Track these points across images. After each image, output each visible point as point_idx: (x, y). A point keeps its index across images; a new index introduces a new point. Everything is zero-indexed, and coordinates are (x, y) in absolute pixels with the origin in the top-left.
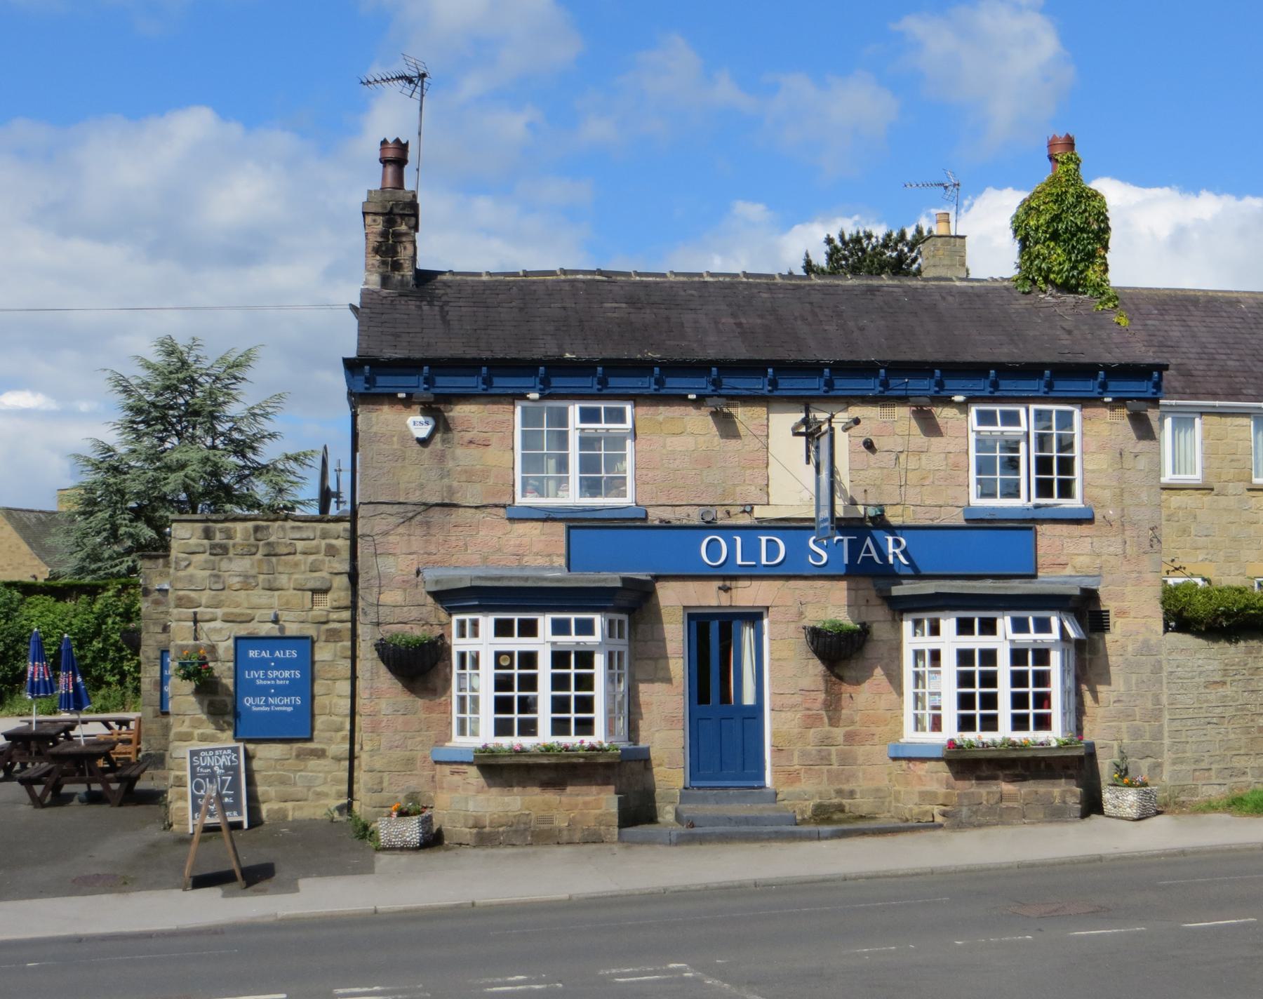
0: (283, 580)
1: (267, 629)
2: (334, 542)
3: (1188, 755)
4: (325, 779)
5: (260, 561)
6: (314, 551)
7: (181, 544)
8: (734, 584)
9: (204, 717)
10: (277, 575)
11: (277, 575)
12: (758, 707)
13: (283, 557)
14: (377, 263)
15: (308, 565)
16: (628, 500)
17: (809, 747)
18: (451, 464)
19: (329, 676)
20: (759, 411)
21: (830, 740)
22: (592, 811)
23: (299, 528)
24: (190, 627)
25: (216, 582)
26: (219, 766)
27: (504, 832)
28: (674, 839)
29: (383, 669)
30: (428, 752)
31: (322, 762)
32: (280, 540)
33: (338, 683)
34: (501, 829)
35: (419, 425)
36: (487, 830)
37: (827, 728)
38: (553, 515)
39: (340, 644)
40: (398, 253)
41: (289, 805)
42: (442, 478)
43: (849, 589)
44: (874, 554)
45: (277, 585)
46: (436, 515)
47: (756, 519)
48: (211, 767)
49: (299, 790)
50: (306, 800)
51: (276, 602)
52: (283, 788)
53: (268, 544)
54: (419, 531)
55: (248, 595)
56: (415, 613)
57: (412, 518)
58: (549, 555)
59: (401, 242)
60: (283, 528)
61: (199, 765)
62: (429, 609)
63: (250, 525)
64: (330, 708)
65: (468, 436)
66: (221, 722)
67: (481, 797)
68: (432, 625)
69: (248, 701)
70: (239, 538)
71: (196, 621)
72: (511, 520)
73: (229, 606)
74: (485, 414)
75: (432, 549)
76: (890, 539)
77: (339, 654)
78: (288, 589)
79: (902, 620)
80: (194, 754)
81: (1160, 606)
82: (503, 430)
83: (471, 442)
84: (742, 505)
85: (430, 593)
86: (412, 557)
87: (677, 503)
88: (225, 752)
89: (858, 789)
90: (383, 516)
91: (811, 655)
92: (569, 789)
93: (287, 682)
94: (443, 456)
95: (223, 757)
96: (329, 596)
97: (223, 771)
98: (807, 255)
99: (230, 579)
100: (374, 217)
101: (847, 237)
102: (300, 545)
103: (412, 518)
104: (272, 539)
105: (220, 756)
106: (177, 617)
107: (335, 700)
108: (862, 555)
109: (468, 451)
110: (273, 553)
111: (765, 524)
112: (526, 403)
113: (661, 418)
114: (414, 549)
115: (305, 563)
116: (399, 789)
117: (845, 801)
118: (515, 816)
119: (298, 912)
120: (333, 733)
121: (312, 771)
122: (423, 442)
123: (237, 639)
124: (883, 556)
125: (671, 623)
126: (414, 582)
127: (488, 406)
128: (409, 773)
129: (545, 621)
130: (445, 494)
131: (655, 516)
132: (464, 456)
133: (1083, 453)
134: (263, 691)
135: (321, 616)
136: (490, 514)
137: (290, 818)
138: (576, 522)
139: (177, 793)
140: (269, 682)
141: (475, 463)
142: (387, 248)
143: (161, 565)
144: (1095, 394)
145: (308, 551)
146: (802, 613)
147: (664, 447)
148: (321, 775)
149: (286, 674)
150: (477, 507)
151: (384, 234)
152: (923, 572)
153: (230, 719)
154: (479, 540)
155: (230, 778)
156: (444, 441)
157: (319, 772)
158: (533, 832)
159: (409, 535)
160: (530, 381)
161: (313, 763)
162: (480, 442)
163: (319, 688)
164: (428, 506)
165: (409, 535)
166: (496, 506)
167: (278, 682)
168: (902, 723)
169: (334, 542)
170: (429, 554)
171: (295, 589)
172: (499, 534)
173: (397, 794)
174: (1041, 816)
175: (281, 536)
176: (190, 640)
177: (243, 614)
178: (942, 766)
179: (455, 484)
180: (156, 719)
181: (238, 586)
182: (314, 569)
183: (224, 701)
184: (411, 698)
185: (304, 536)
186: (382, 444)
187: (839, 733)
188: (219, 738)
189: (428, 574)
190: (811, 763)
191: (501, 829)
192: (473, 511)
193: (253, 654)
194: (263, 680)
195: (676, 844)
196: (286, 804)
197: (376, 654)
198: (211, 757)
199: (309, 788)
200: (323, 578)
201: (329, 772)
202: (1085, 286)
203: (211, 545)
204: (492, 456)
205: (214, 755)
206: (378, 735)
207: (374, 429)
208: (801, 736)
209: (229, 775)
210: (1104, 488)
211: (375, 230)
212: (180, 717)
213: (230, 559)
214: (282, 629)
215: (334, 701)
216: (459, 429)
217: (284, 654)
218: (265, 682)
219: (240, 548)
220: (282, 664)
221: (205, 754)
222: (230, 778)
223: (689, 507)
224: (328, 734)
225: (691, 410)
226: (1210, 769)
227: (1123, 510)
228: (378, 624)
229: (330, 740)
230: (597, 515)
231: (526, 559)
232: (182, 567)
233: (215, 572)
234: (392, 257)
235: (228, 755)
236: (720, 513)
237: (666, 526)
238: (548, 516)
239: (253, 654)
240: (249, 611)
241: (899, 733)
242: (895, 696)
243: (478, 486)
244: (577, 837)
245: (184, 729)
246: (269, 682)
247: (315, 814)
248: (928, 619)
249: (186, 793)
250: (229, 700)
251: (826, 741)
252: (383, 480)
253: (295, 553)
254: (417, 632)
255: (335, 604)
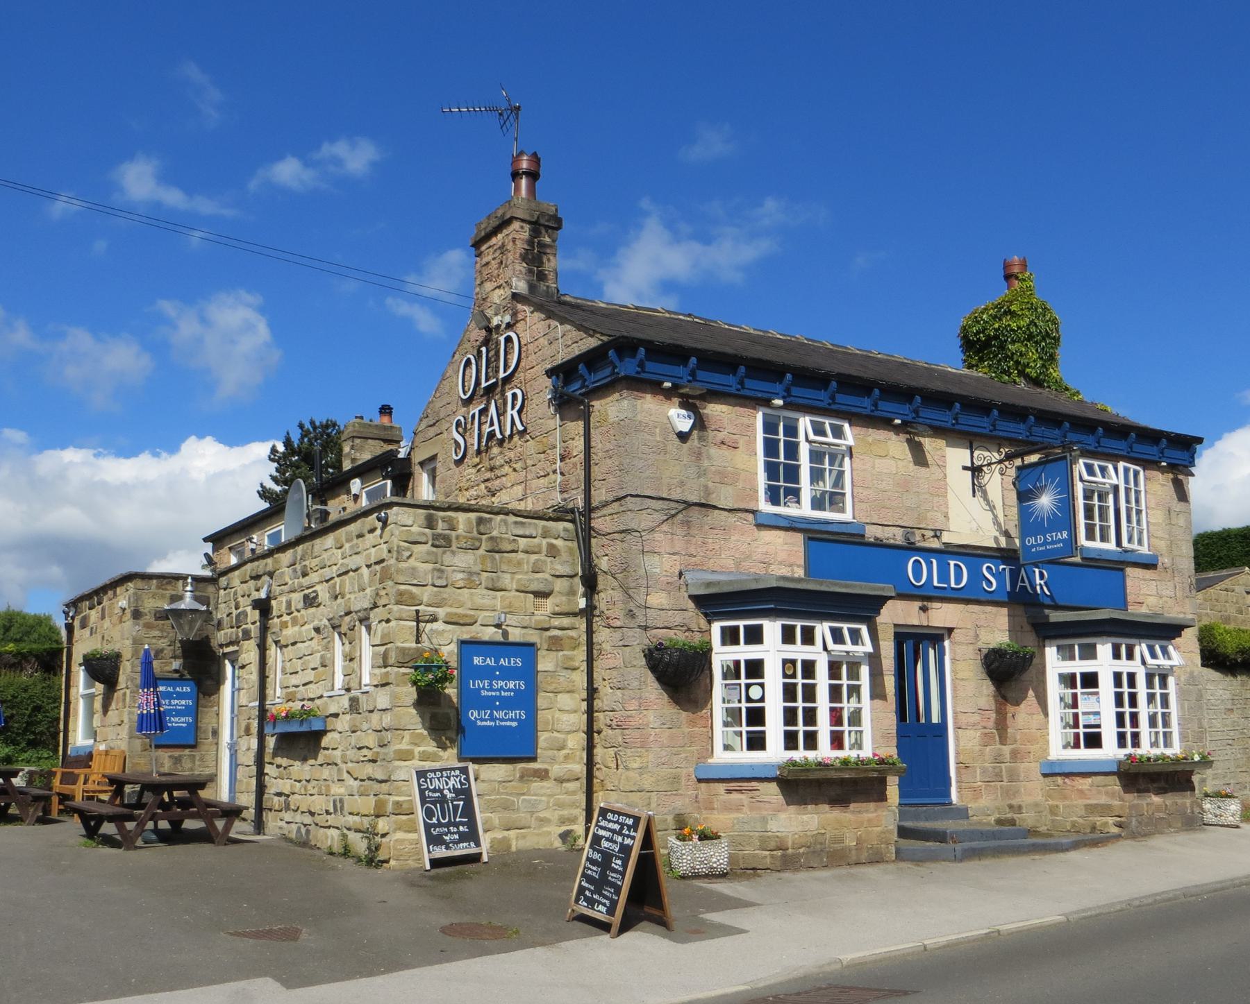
0: (506, 580)
1: (489, 634)
2: (554, 542)
3: (1220, 771)
4: (548, 802)
5: (483, 557)
6: (536, 550)
7: (403, 531)
8: (929, 605)
9: (425, 733)
10: (499, 573)
11: (499, 573)
12: (943, 726)
13: (505, 554)
14: (524, 270)
15: (531, 565)
16: (847, 516)
17: (986, 765)
18: (706, 463)
19: (551, 688)
20: (941, 443)
21: (1001, 757)
22: (874, 829)
23: (522, 523)
24: (411, 628)
25: (439, 578)
26: (449, 789)
27: (803, 853)
28: (958, 854)
29: (650, 678)
30: (691, 769)
31: (545, 784)
32: (503, 536)
33: (560, 696)
34: (801, 851)
35: (683, 421)
36: (790, 851)
37: (999, 746)
38: (797, 525)
39: (561, 653)
40: (543, 263)
41: (512, 833)
42: (699, 477)
43: (1009, 615)
44: (1027, 584)
45: (499, 585)
46: (695, 513)
47: (944, 543)
48: (441, 791)
49: (522, 816)
50: (529, 827)
51: (499, 604)
52: (506, 814)
53: (492, 539)
54: (680, 531)
55: (472, 594)
56: (678, 618)
57: (673, 516)
58: (791, 565)
59: (545, 253)
60: (505, 522)
61: (428, 788)
62: (691, 614)
63: (473, 516)
64: (553, 724)
65: (721, 436)
66: (444, 738)
67: (783, 816)
68: (693, 632)
69: (473, 714)
70: (461, 528)
71: (418, 621)
72: (760, 526)
73: (451, 606)
74: (733, 415)
75: (692, 550)
76: (1037, 571)
77: (560, 664)
78: (510, 590)
79: (1044, 647)
80: (421, 774)
81: (1198, 643)
82: (749, 434)
83: (723, 443)
84: (932, 530)
85: (693, 597)
86: (675, 557)
87: (886, 523)
88: (453, 773)
89: (1023, 805)
90: (649, 510)
91: (984, 676)
92: (852, 806)
93: (512, 694)
94: (700, 454)
95: (452, 778)
96: (550, 601)
97: (454, 795)
98: (288, 433)
99: (454, 576)
100: (522, 224)
101: (318, 424)
102: (522, 542)
103: (673, 516)
104: (495, 533)
105: (449, 778)
106: (397, 616)
107: (557, 714)
108: (1019, 584)
109: (721, 452)
110: (497, 549)
111: (950, 549)
112: (768, 411)
113: (870, 439)
114: (677, 549)
115: (528, 562)
116: (666, 810)
117: (1015, 816)
118: (813, 836)
119: (867, 953)
120: (555, 752)
121: (536, 795)
122: (683, 437)
123: (463, 643)
124: (1034, 588)
125: (885, 640)
126: (678, 585)
127: (736, 408)
128: (674, 792)
129: (822, 629)
130: (702, 494)
131: (872, 533)
132: (717, 456)
133: (1147, 508)
134: (488, 703)
135: (545, 621)
136: (741, 518)
137: (514, 849)
138: (815, 534)
139: (395, 822)
140: (494, 694)
141: (727, 464)
142: (533, 257)
143: (153, 587)
144: (1156, 458)
145: (529, 549)
146: (977, 636)
147: (873, 467)
148: (543, 798)
149: (511, 685)
150: (730, 510)
151: (530, 242)
152: (1061, 603)
153: (452, 734)
154: (732, 546)
155: (462, 803)
156: (700, 438)
157: (542, 796)
158: (828, 852)
159: (672, 534)
160: (778, 387)
161: (536, 785)
162: (730, 444)
163: (542, 700)
164: (689, 505)
165: (672, 534)
166: (747, 511)
167: (503, 694)
168: (1048, 742)
169: (554, 542)
170: (691, 555)
171: (517, 591)
172: (749, 540)
173: (666, 817)
174: (1180, 825)
175: (504, 531)
176: (412, 643)
177: (466, 616)
178: (1115, 779)
179: (710, 484)
180: (145, 753)
181: (461, 584)
182: (537, 570)
183: (447, 714)
184: (675, 710)
185: (527, 533)
186: (646, 434)
187: (1006, 750)
188: (441, 757)
189: (688, 576)
190: (989, 779)
191: (801, 851)
192: (726, 513)
193: (477, 661)
194: (488, 690)
195: (961, 861)
196: (509, 832)
197: (643, 662)
198: (438, 779)
199: (532, 813)
200: (546, 580)
201: (551, 796)
202: (1049, 381)
203: (433, 535)
204: (739, 459)
205: (442, 777)
206: (647, 751)
207: (639, 418)
208: (982, 753)
209: (460, 800)
210: (1161, 539)
211: (522, 237)
212: (399, 732)
213: (453, 553)
214: (505, 634)
215: (557, 716)
216: (713, 427)
217: (509, 663)
218: (490, 694)
219: (465, 540)
220: (508, 674)
221: (432, 775)
222: (462, 803)
223: (894, 528)
224: (550, 753)
225: (892, 435)
226: (1230, 784)
227: (1173, 559)
228: (645, 628)
229: (553, 760)
230: (816, 527)
231: (772, 567)
232: (405, 558)
233: (438, 566)
234: (537, 267)
235: (457, 777)
236: (917, 538)
237: (879, 544)
238: (791, 526)
239: (477, 661)
240: (472, 613)
241: (1046, 750)
242: (1043, 717)
243: (729, 488)
244: (863, 858)
245: (404, 746)
246: (494, 694)
247: (538, 843)
248: (1079, 645)
249: (414, 822)
250: (452, 714)
251: (998, 759)
252: (648, 473)
253: (517, 552)
254: (680, 637)
255: (557, 609)
